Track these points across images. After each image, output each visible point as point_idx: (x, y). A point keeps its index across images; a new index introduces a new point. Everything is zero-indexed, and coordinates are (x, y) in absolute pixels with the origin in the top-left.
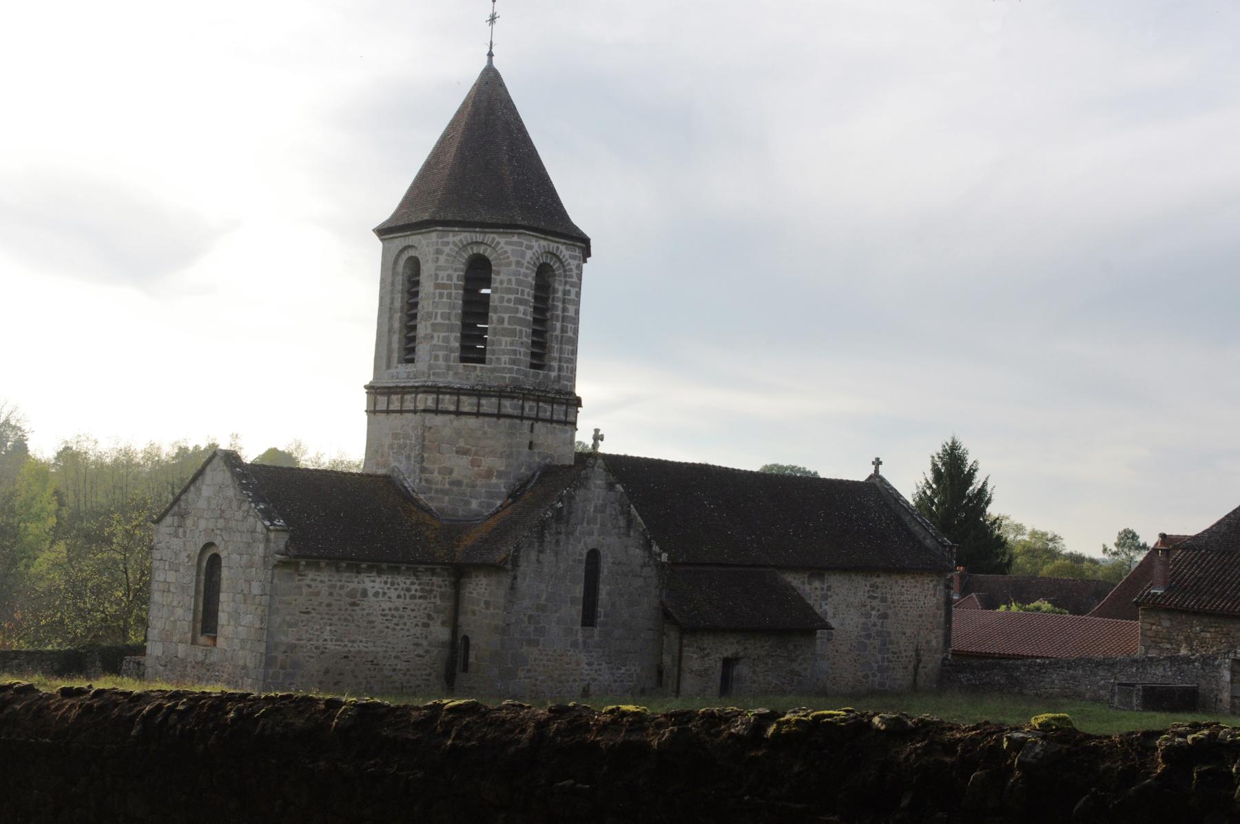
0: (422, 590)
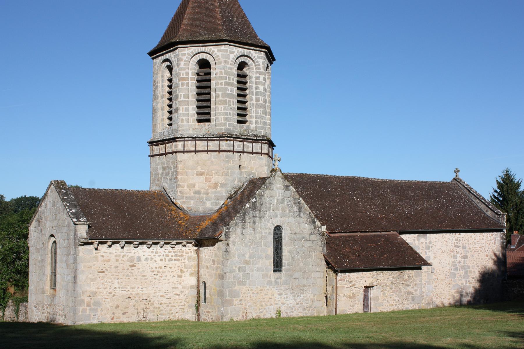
0: (176, 255)
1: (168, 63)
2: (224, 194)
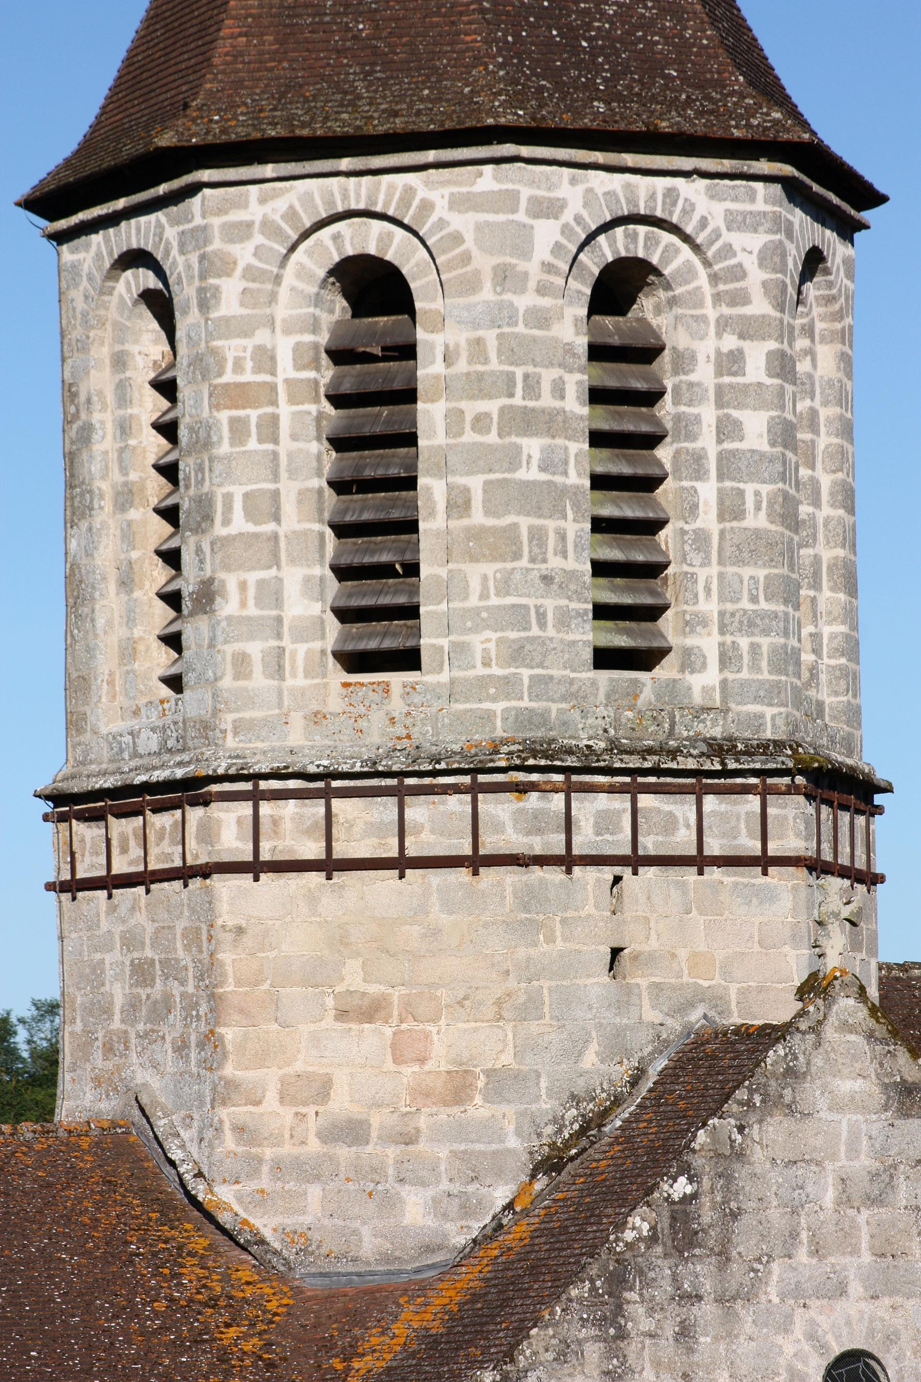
1: (151, 280)
2: (513, 1142)
